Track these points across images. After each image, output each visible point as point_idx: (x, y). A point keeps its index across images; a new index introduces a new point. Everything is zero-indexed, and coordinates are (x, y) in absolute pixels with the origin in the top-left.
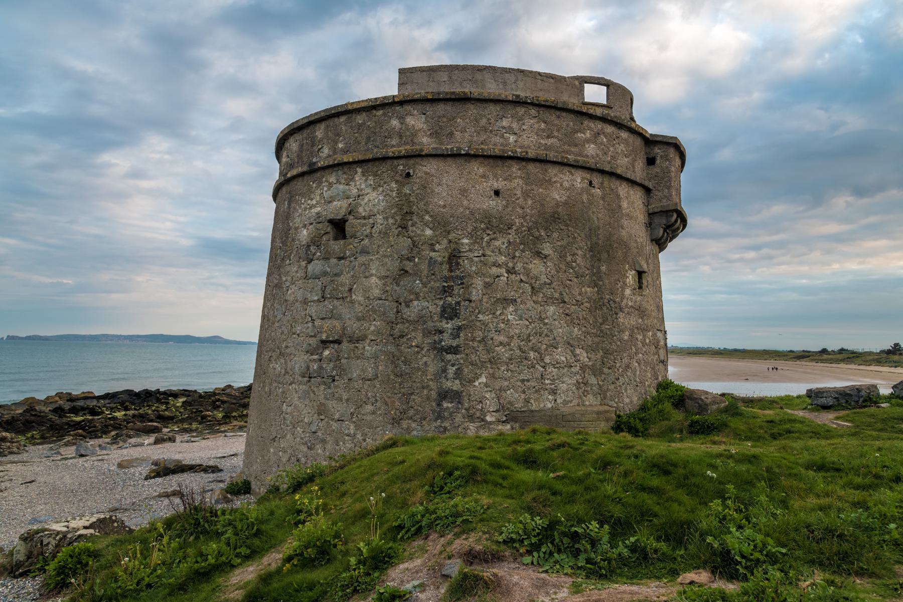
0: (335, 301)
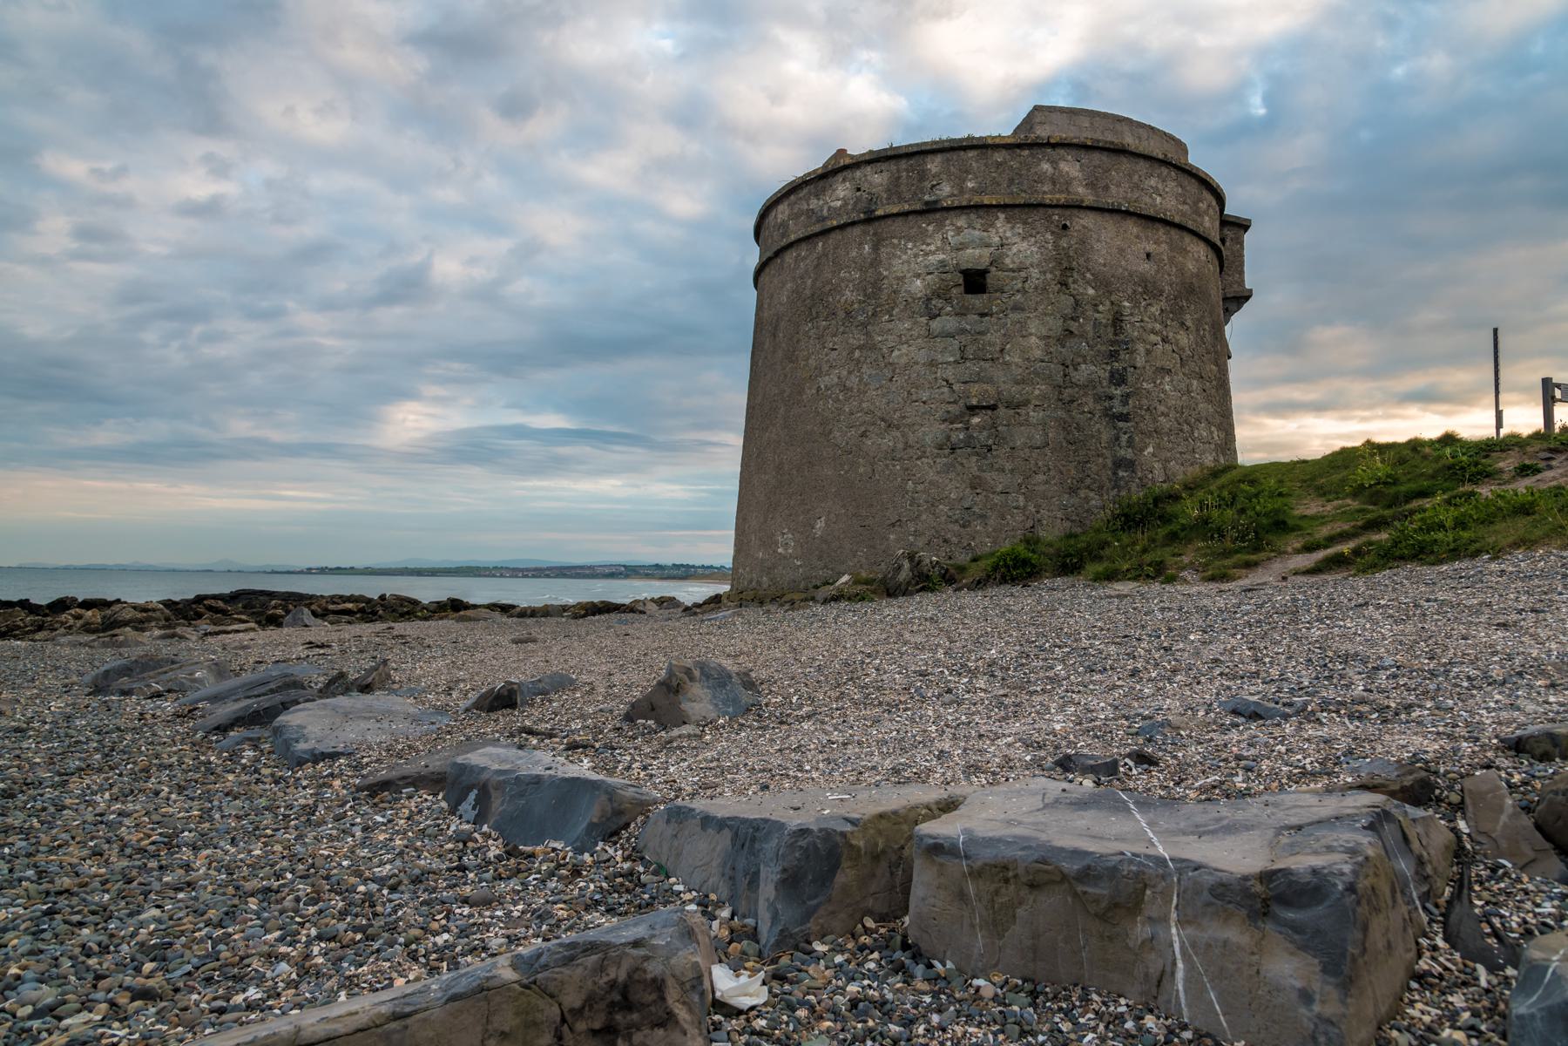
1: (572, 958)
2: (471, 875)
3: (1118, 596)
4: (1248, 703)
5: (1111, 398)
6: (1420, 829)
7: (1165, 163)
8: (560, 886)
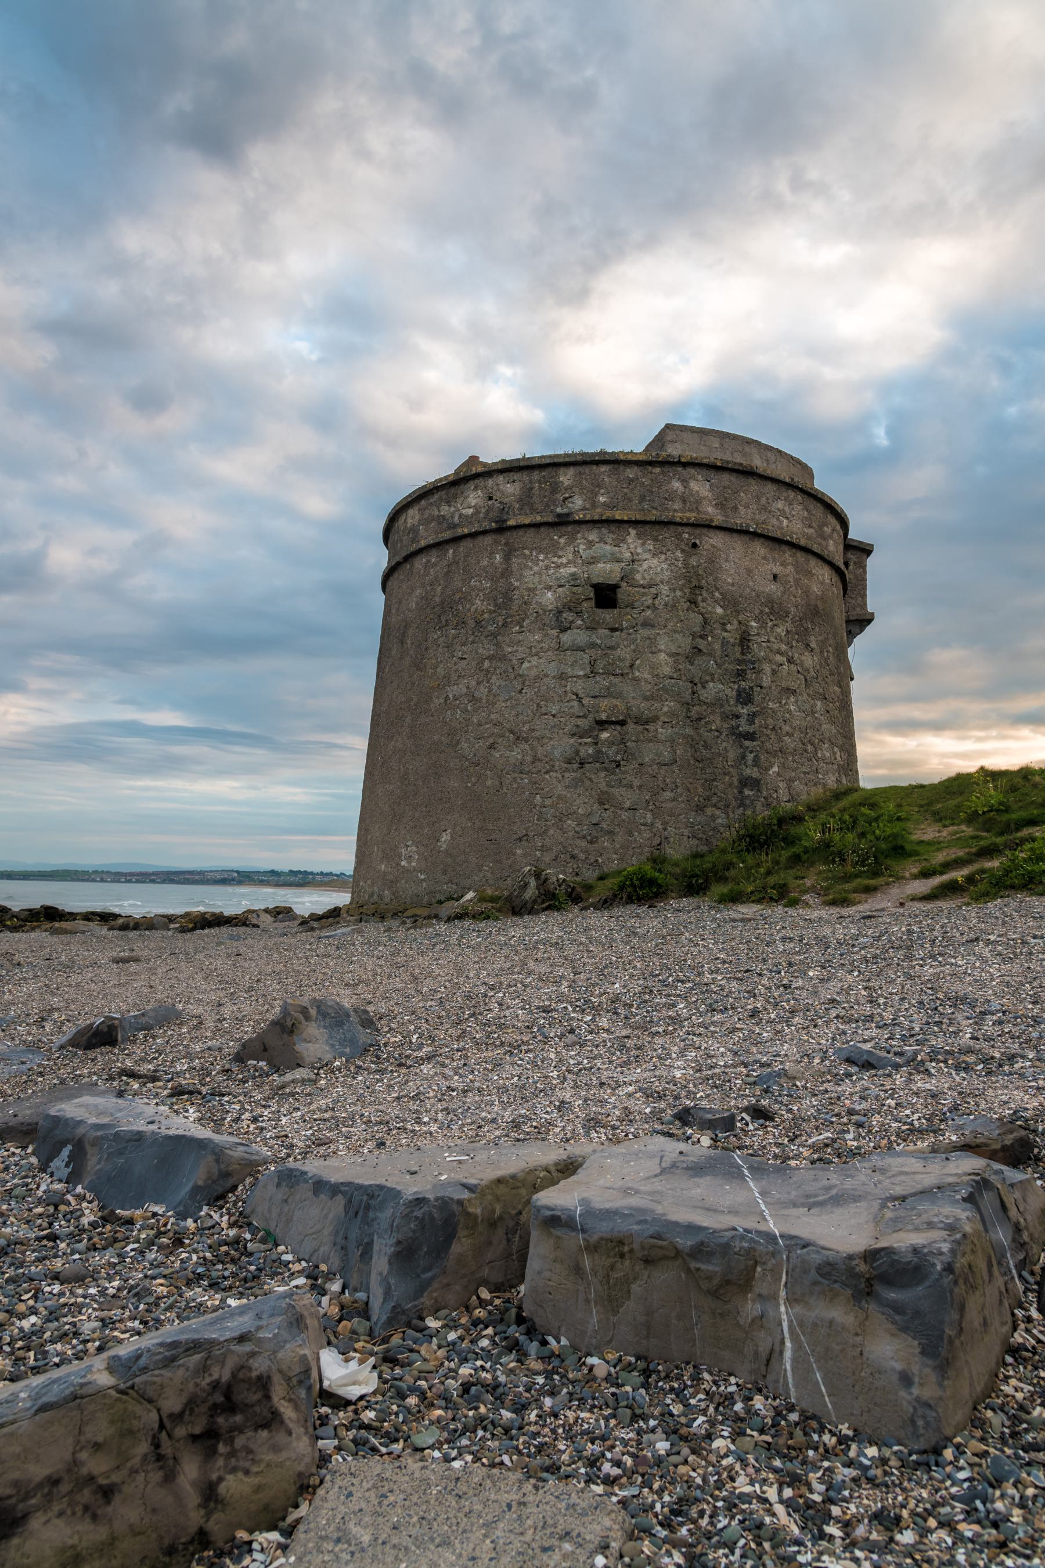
0: (612, 678)
1: (173, 1359)
2: (63, 1245)
3: (742, 920)
4: (861, 1052)
5: (738, 717)
6: (1017, 1195)
7: (791, 486)
8: (161, 1258)
